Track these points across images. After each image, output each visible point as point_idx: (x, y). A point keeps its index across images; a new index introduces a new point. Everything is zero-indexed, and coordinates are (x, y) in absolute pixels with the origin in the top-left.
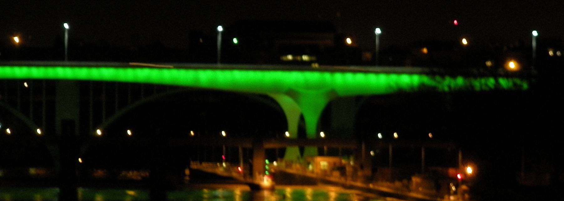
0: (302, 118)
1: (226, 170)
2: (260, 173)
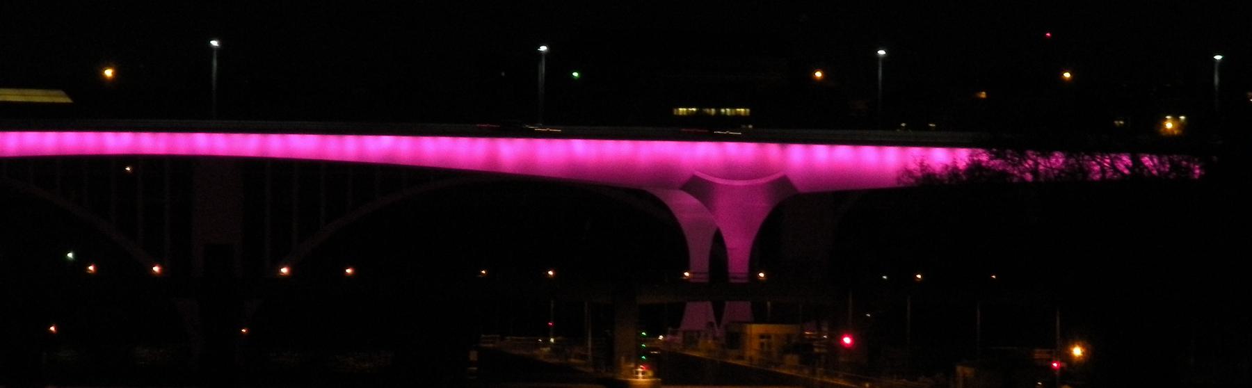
0: (718, 238)
1: (556, 349)
2: (628, 360)
